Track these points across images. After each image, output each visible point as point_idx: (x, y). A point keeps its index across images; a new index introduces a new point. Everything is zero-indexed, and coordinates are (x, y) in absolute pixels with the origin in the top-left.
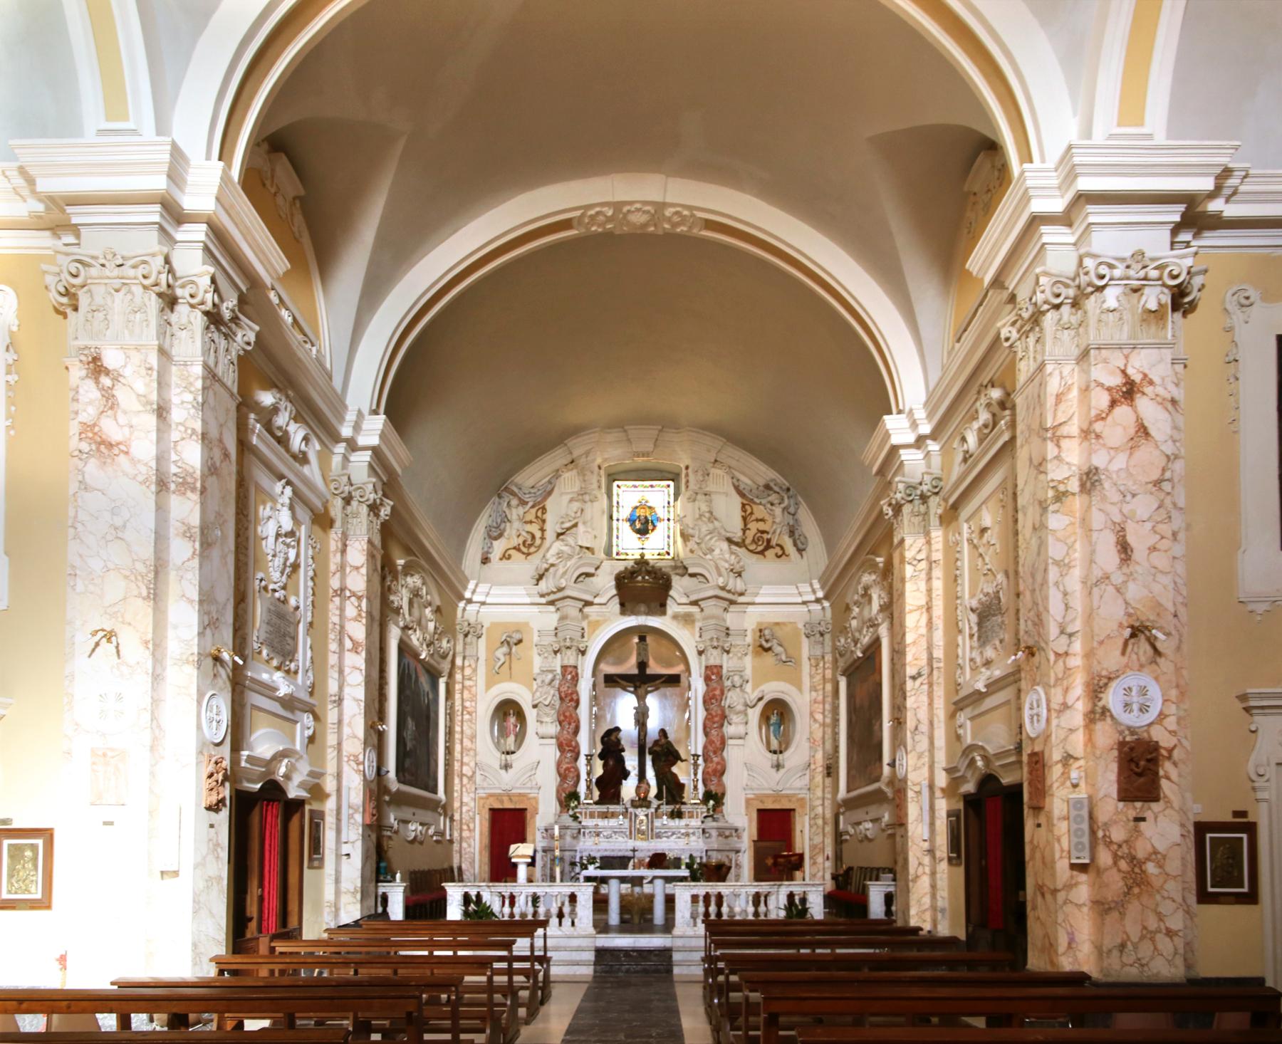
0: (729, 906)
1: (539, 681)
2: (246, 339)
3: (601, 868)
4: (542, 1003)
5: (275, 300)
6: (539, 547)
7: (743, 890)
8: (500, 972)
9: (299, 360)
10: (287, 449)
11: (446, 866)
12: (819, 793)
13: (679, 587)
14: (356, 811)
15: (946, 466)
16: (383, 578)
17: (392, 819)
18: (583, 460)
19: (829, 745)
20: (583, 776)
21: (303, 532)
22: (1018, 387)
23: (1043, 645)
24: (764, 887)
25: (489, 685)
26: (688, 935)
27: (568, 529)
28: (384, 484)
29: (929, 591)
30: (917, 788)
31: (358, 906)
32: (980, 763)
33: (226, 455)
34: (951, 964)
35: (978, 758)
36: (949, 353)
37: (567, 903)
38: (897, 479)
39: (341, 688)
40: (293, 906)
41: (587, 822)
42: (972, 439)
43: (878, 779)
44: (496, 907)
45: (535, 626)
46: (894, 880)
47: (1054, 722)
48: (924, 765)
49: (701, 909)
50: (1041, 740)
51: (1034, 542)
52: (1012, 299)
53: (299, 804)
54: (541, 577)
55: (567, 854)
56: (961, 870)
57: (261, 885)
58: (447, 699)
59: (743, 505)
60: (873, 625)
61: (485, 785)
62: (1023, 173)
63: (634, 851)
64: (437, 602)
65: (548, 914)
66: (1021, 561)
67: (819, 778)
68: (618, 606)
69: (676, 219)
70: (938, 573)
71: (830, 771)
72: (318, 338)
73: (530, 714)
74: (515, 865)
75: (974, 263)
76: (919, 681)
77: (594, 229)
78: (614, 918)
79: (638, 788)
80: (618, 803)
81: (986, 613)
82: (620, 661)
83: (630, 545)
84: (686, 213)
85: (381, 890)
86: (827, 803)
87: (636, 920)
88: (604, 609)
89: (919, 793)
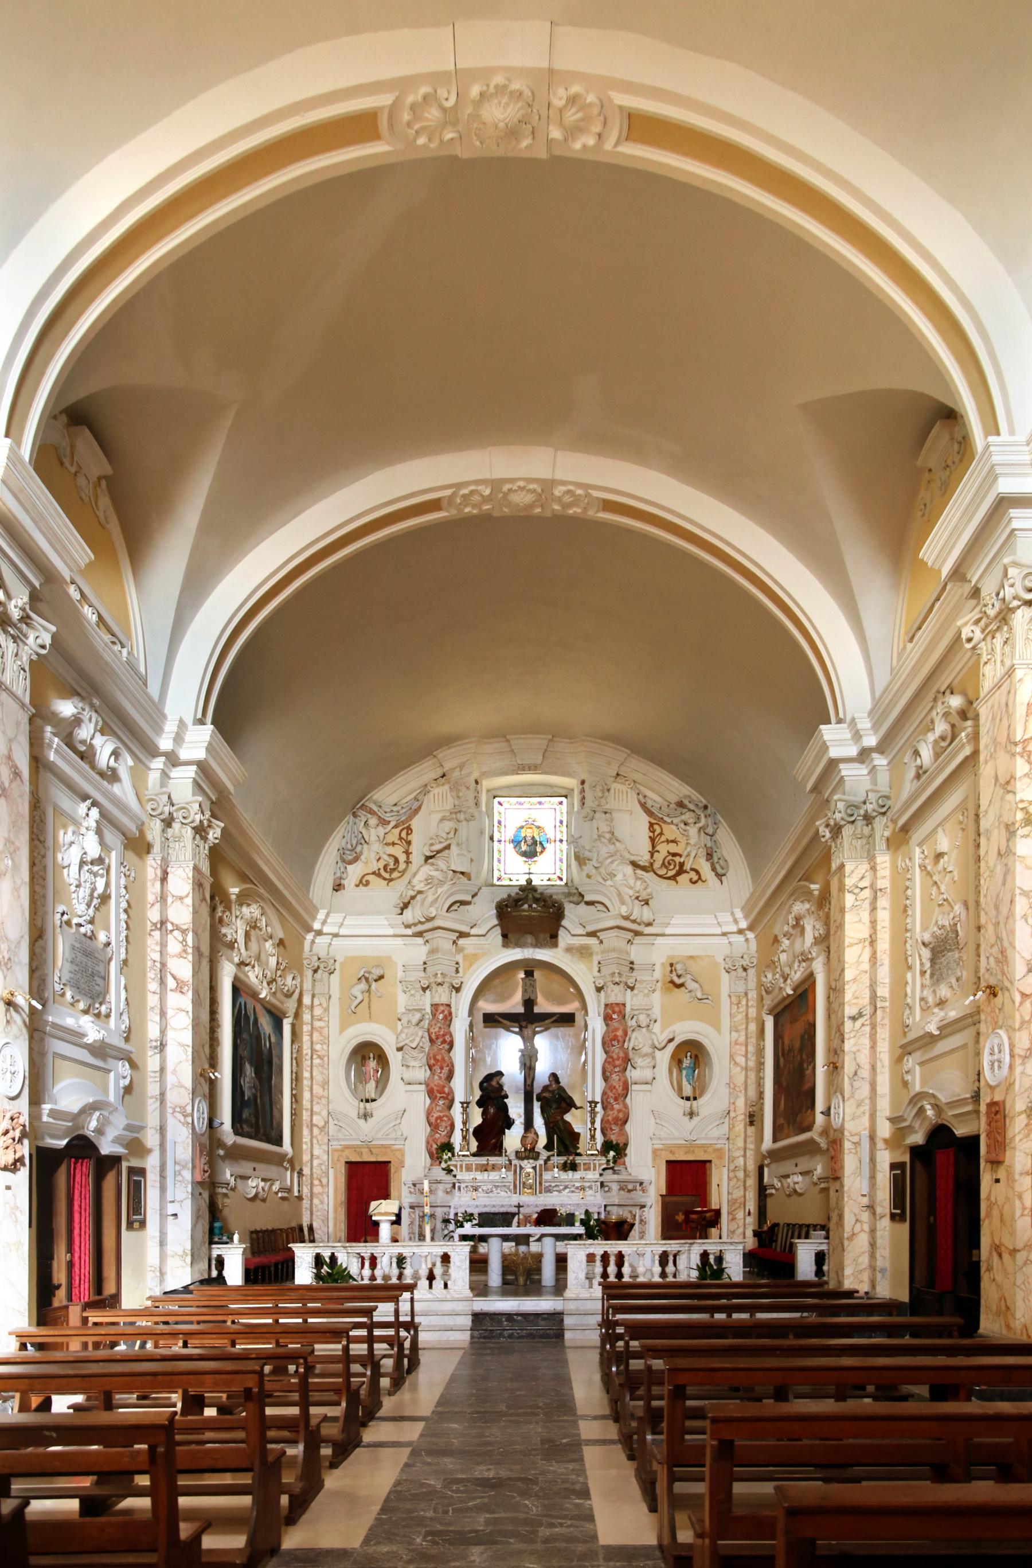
0: (631, 1266)
1: (404, 1021)
2: (39, 641)
3: (480, 1225)
4: (409, 1371)
5: (75, 595)
6: (404, 872)
7: (648, 1249)
8: (358, 1340)
9: (107, 663)
10: (93, 766)
11: (293, 1224)
12: (741, 1144)
13: (574, 918)
14: (184, 1167)
15: (896, 782)
16: (213, 909)
17: (227, 1174)
18: (456, 774)
19: (752, 1092)
20: (459, 1125)
21: (113, 859)
22: (982, 695)
23: (1007, 984)
24: (672, 1246)
25: (344, 1026)
26: (582, 1299)
27: (438, 852)
28: (212, 802)
29: (873, 923)
30: (856, 1139)
31: (189, 1269)
32: (930, 1113)
33: (17, 774)
34: (890, 1330)
35: (928, 1107)
36: (900, 655)
37: (439, 1264)
38: (836, 797)
39: (163, 1032)
40: (109, 1272)
41: (463, 1176)
42: (926, 753)
43: (809, 1128)
44: (354, 1269)
45: (399, 960)
46: (827, 1237)
47: (1018, 1069)
48: (866, 1112)
49: (598, 1269)
50: (1003, 1087)
51: (999, 870)
52: (976, 593)
53: (115, 1161)
54: (406, 906)
55: (439, 1210)
56: (906, 1227)
57: (70, 1249)
58: (293, 1042)
59: (651, 825)
60: (806, 959)
61: (340, 1136)
62: (987, 446)
63: (519, 1206)
64: (280, 934)
65: (416, 1277)
66: (983, 892)
67: (740, 1127)
68: (499, 939)
69: (567, 499)
70: (883, 902)
71: (753, 1119)
72: (129, 637)
73: (394, 1058)
74: (376, 1224)
75: (928, 553)
76: (858, 1023)
77: (467, 510)
78: (495, 1277)
79: (524, 1138)
80: (500, 1155)
81: (941, 949)
82: (503, 998)
83: (512, 871)
84: (579, 492)
85: (215, 1253)
86: (749, 1153)
87: (521, 1280)
89: (857, 1144)
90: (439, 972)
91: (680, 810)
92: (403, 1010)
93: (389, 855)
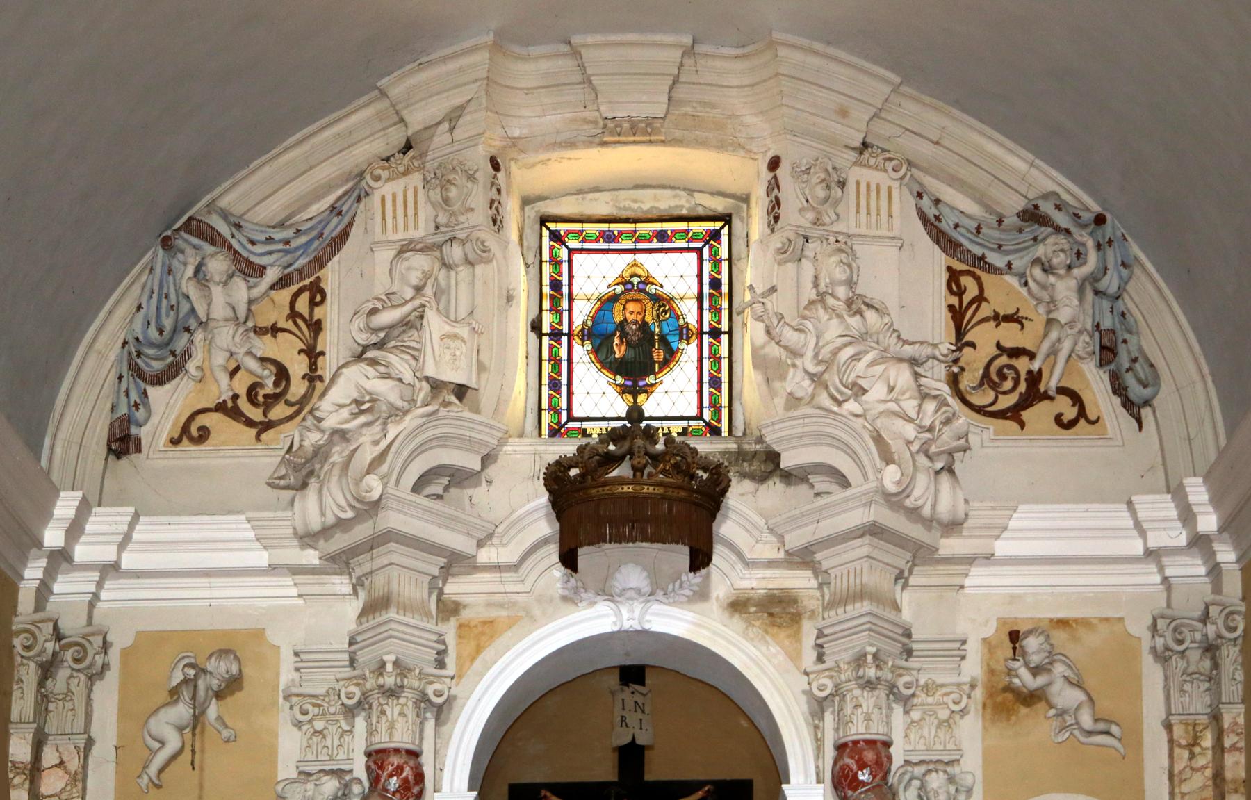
13: (745, 514)
18: (441, 137)
45: (284, 640)
59: (954, 276)
88: (511, 584)
90: (390, 658)
91: (1032, 229)
92: (294, 774)
93: (263, 360)
